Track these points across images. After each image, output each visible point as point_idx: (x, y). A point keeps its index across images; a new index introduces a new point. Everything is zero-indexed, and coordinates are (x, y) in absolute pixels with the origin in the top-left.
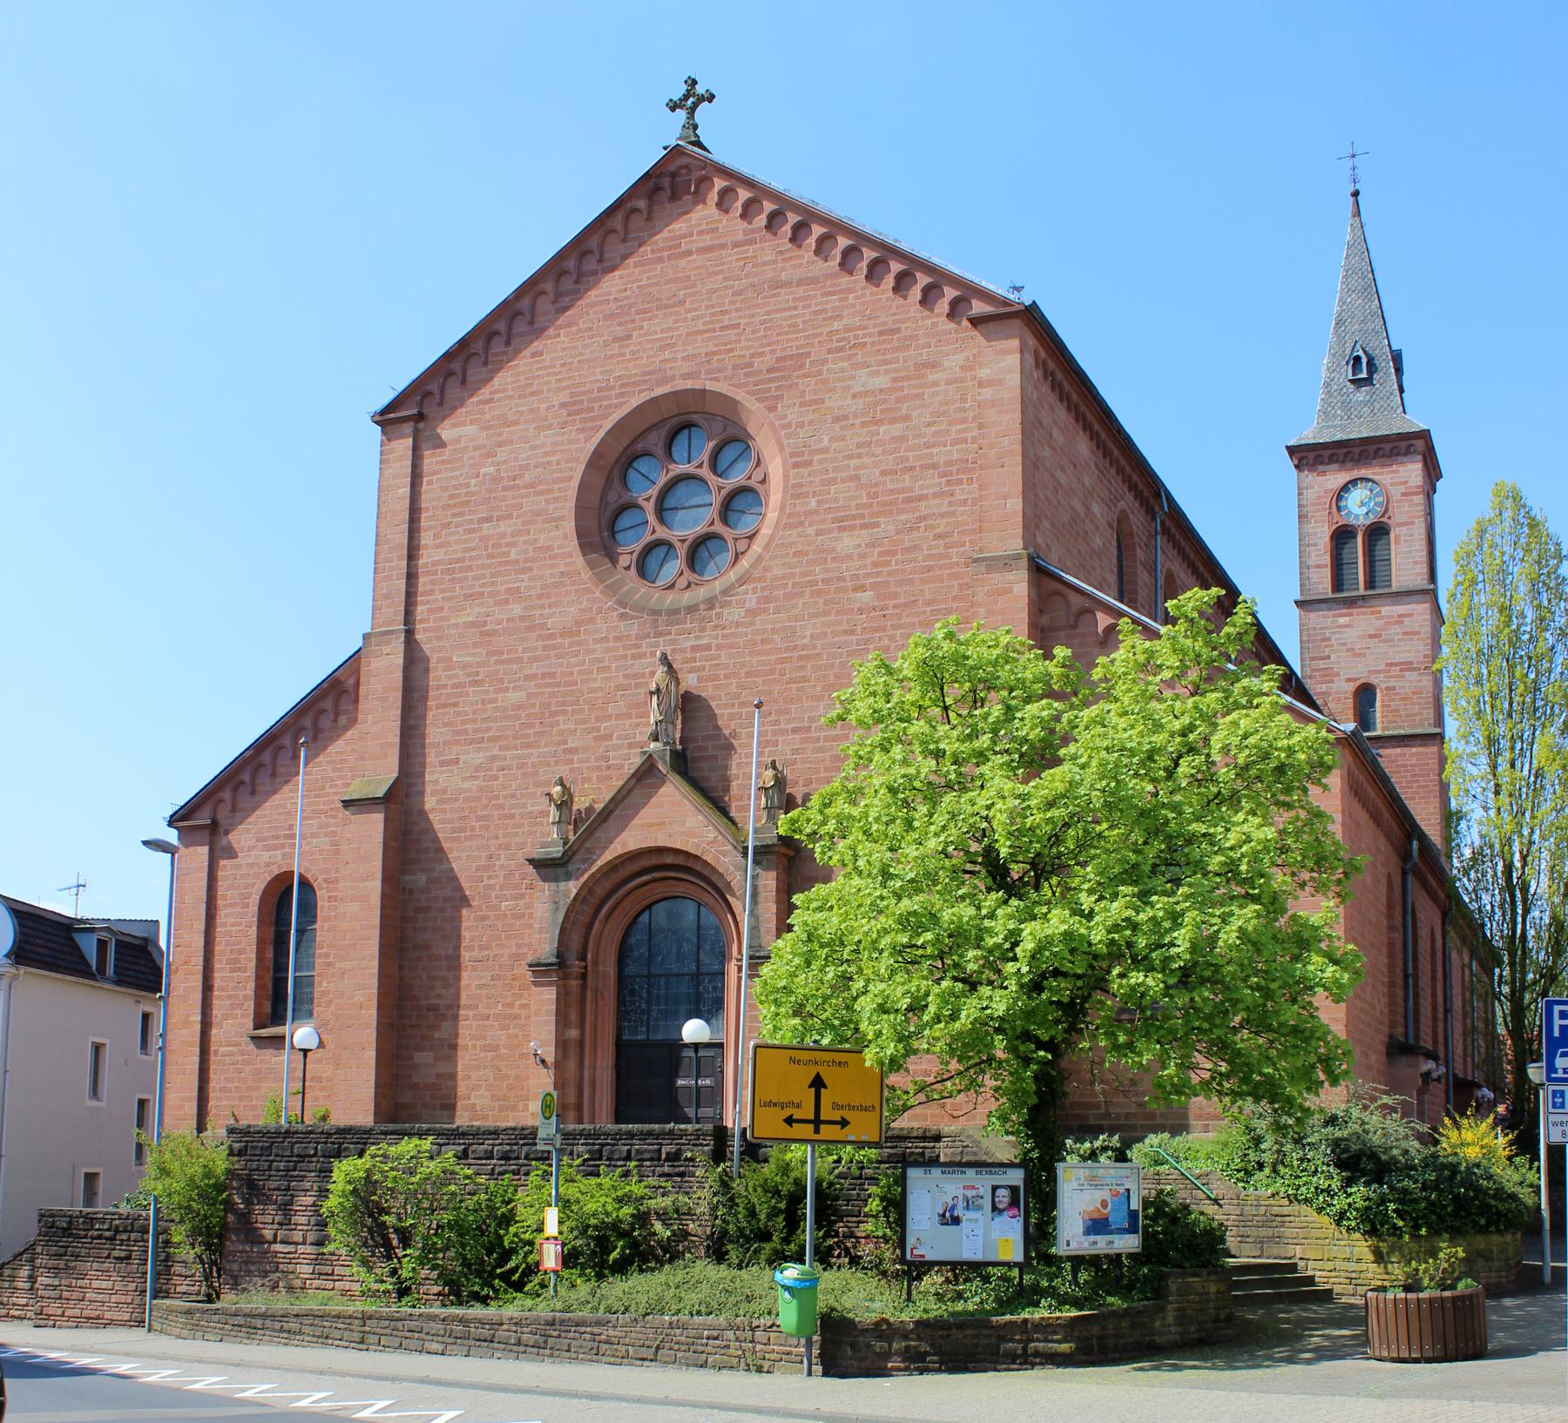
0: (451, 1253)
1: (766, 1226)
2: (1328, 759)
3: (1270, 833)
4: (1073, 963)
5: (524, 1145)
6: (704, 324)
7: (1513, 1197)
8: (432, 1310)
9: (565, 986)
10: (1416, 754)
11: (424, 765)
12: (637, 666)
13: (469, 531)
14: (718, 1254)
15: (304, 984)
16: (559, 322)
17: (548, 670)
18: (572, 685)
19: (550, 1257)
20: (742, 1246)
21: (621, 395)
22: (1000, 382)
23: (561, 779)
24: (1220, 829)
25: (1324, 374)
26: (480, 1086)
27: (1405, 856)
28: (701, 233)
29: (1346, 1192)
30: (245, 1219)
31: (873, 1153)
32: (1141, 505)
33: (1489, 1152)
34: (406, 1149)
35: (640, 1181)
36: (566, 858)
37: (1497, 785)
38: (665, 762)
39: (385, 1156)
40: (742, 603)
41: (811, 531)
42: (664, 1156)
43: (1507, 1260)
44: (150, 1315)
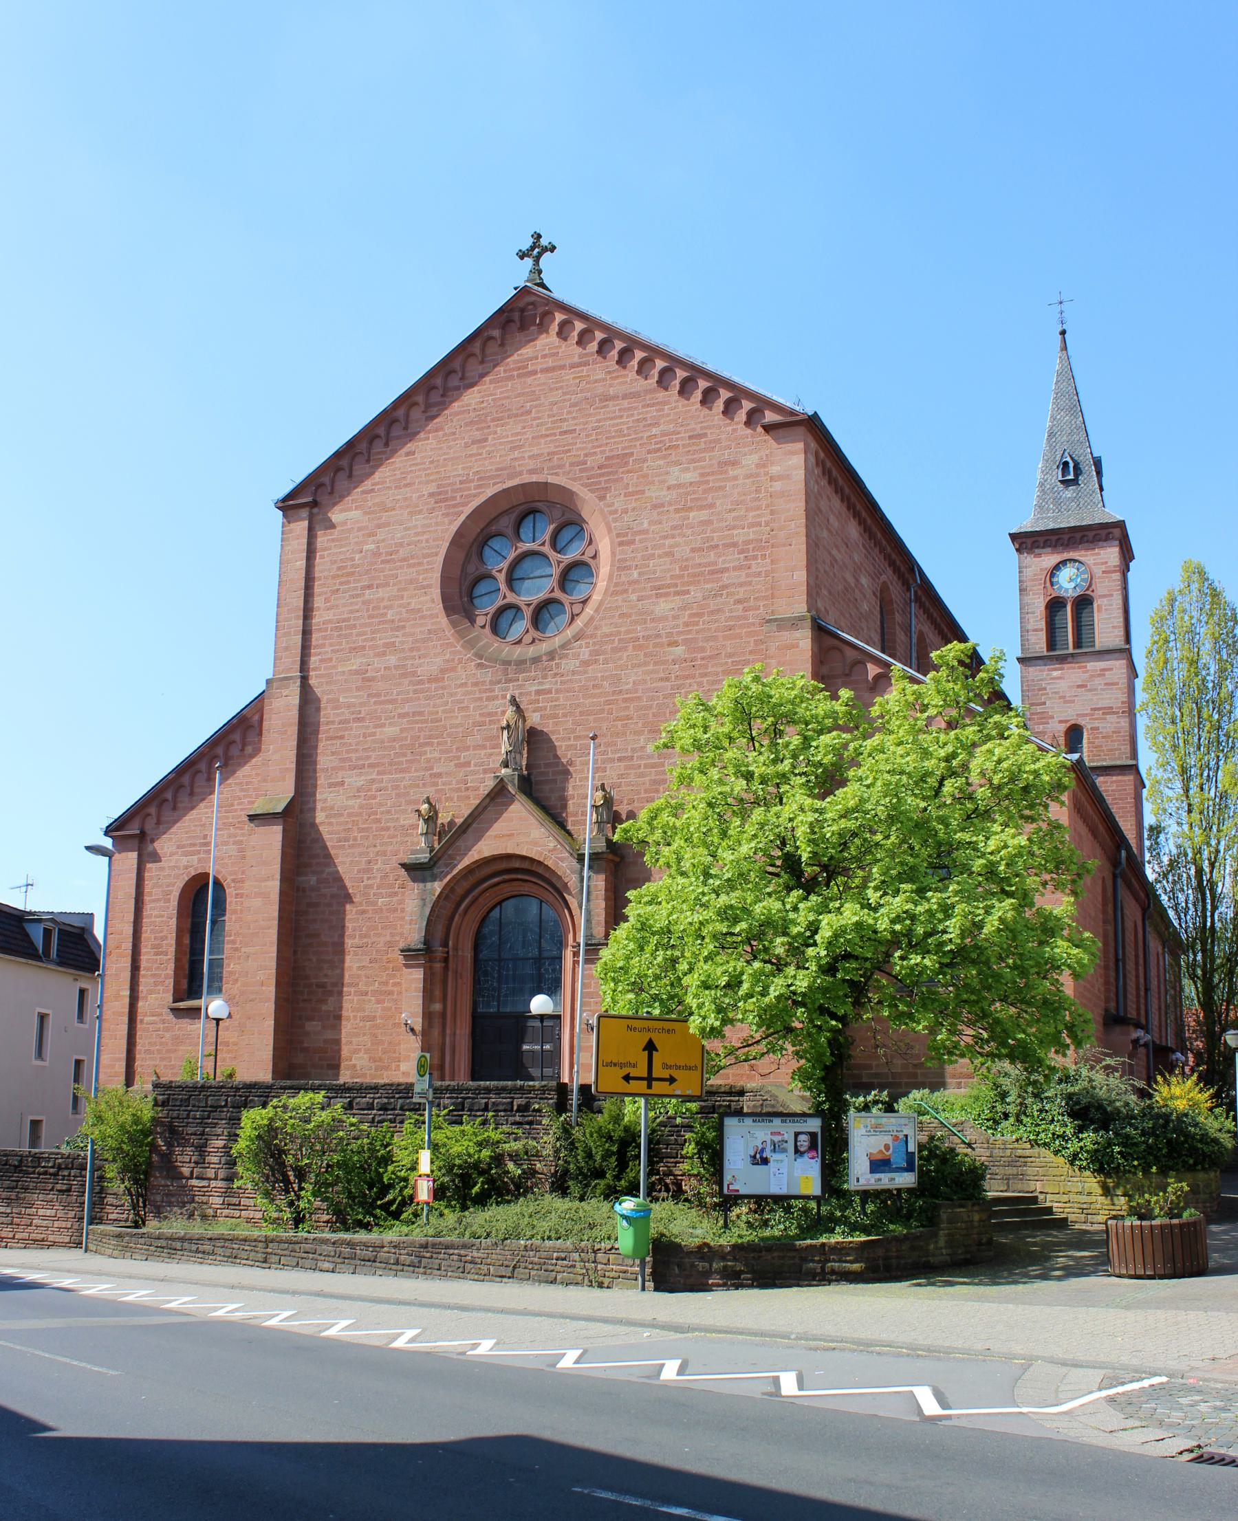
0: (339, 1188)
1: (601, 1166)
2: (1066, 780)
3: (1023, 840)
4: (862, 948)
5: (400, 1098)
6: (546, 429)
7: (1215, 1141)
8: (324, 1235)
9: (431, 968)
10: (1115, 782)
11: (315, 786)
12: (492, 706)
13: (352, 597)
14: (560, 1186)
15: (216, 965)
16: (429, 428)
17: (418, 710)
18: (437, 721)
19: (424, 1191)
20: (581, 1183)
21: (479, 486)
22: (788, 477)
23: (428, 798)
24: (981, 838)
25: (1039, 476)
26: (360, 1050)
27: (1115, 862)
28: (544, 356)
29: (1078, 1137)
30: (167, 1159)
31: (694, 1106)
32: (899, 579)
33: (1194, 1105)
34: (303, 1101)
35: (496, 1129)
36: (432, 863)
37: (1190, 805)
38: (514, 785)
39: (285, 1107)
40: (576, 656)
41: (634, 597)
42: (515, 1108)
43: (1211, 1193)
44: (87, 1238)
